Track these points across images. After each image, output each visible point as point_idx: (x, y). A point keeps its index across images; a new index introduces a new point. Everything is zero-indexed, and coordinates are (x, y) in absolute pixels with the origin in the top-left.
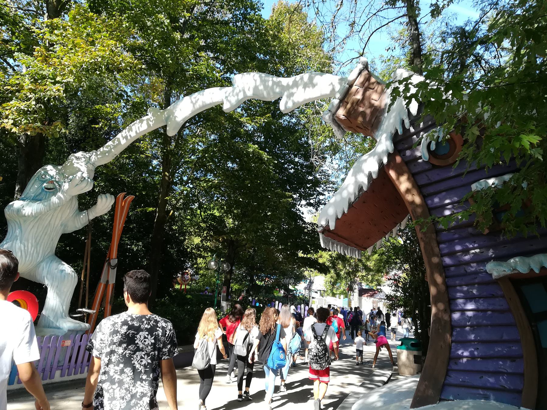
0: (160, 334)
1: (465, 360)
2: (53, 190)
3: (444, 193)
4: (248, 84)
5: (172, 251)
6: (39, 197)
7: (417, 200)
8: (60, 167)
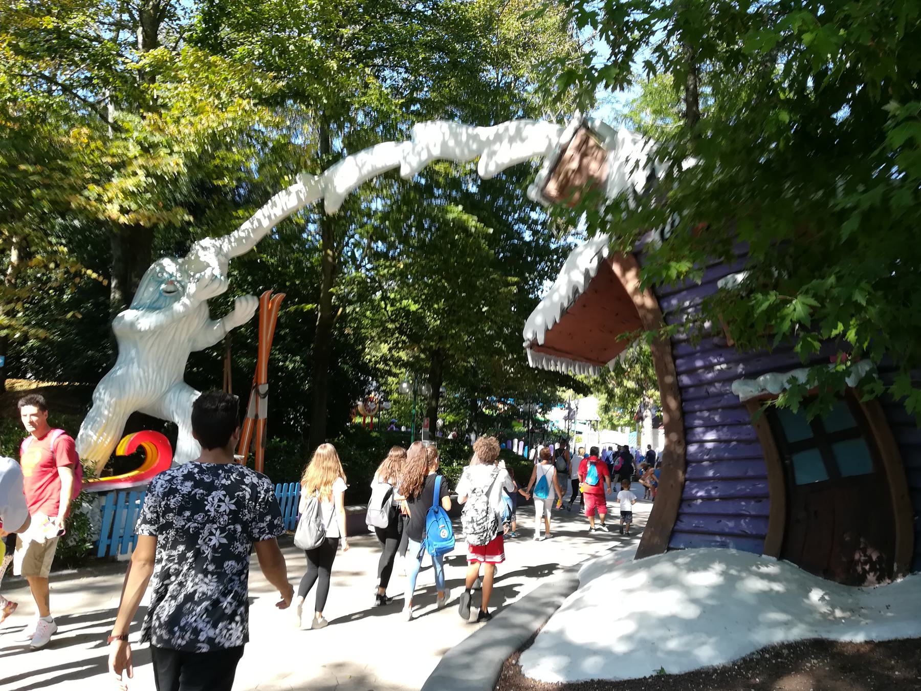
0: (248, 497)
1: (699, 501)
2: (175, 293)
3: (684, 293)
4: (430, 140)
5: (346, 367)
6: (157, 305)
7: (649, 302)
8: (180, 260)
